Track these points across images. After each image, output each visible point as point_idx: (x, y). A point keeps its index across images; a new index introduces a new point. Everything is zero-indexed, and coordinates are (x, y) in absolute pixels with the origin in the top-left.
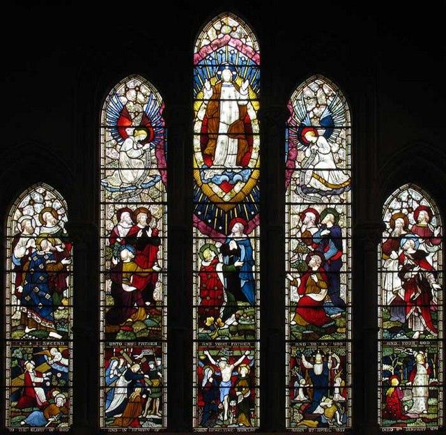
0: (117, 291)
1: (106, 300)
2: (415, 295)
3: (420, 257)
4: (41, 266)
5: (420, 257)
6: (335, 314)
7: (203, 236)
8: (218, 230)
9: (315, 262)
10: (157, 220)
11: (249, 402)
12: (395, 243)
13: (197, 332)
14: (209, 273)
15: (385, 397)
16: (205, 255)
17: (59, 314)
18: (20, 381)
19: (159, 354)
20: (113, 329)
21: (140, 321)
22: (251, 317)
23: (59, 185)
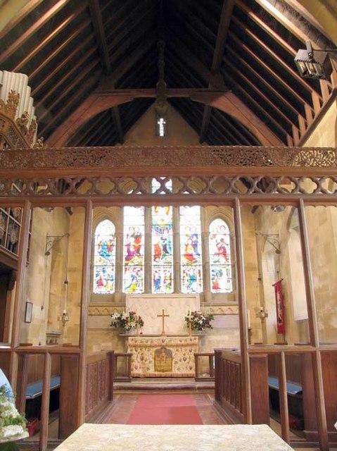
0: (129, 251)
1: (125, 254)
2: (221, 251)
3: (222, 240)
4: (201, 322)
5: (222, 240)
6: (196, 257)
7: (171, 349)
8: (160, 231)
9: (190, 242)
10: (141, 230)
11: (170, 284)
12: (214, 236)
13: (153, 263)
14: (156, 246)
15: (213, 283)
16: (156, 239)
17: (110, 258)
18: (98, 278)
19: (141, 269)
20: (127, 262)
21: (136, 260)
22: (170, 258)
23: (114, 221)
